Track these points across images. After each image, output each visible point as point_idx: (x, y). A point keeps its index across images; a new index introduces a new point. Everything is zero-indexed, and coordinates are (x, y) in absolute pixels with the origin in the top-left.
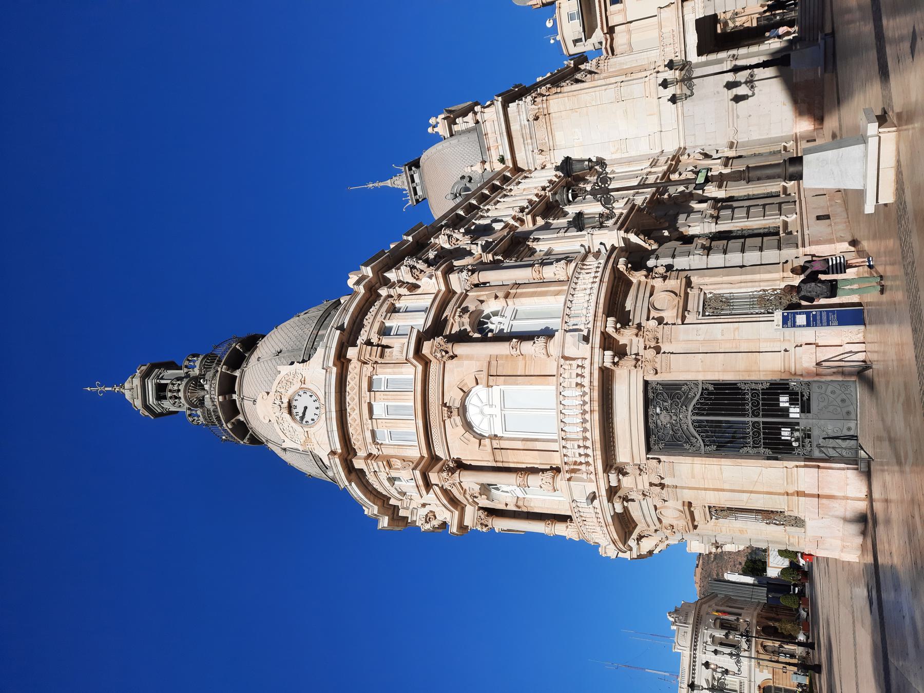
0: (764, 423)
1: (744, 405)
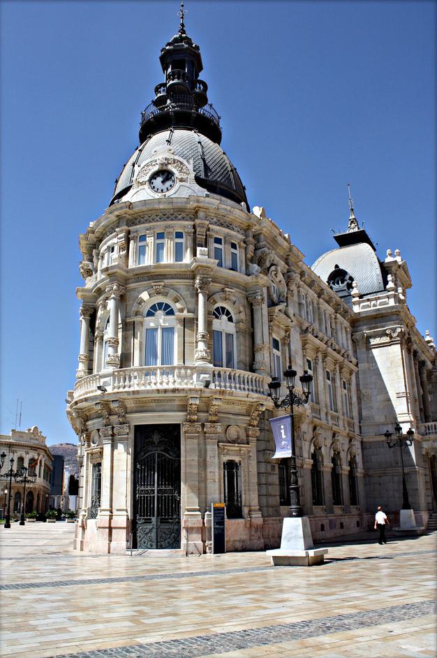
0: (154, 497)
1: (150, 485)
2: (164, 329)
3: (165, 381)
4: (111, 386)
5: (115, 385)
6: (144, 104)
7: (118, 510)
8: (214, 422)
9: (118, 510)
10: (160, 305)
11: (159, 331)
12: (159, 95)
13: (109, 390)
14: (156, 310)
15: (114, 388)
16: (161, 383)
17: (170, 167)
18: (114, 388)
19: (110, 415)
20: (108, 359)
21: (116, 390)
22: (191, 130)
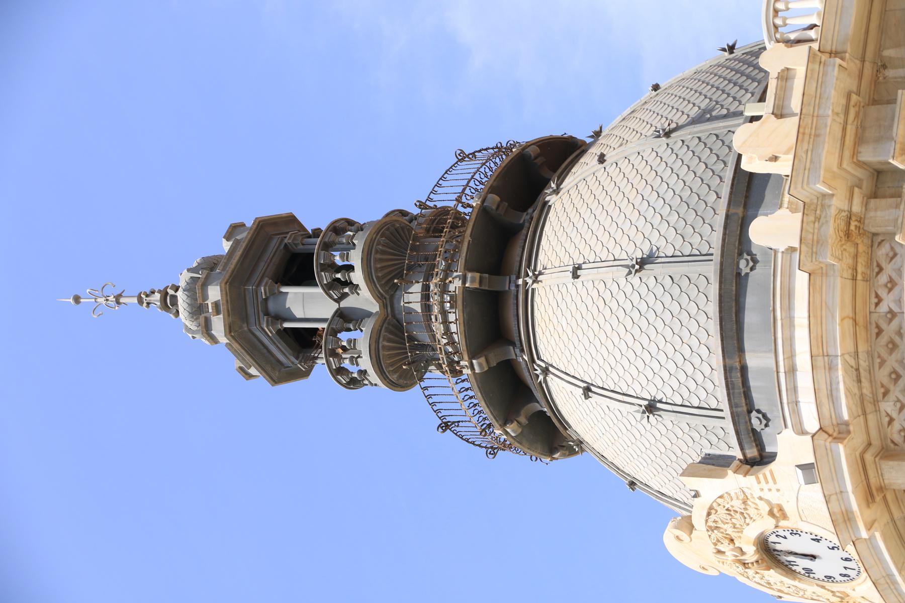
12: (357, 276)
17: (751, 553)
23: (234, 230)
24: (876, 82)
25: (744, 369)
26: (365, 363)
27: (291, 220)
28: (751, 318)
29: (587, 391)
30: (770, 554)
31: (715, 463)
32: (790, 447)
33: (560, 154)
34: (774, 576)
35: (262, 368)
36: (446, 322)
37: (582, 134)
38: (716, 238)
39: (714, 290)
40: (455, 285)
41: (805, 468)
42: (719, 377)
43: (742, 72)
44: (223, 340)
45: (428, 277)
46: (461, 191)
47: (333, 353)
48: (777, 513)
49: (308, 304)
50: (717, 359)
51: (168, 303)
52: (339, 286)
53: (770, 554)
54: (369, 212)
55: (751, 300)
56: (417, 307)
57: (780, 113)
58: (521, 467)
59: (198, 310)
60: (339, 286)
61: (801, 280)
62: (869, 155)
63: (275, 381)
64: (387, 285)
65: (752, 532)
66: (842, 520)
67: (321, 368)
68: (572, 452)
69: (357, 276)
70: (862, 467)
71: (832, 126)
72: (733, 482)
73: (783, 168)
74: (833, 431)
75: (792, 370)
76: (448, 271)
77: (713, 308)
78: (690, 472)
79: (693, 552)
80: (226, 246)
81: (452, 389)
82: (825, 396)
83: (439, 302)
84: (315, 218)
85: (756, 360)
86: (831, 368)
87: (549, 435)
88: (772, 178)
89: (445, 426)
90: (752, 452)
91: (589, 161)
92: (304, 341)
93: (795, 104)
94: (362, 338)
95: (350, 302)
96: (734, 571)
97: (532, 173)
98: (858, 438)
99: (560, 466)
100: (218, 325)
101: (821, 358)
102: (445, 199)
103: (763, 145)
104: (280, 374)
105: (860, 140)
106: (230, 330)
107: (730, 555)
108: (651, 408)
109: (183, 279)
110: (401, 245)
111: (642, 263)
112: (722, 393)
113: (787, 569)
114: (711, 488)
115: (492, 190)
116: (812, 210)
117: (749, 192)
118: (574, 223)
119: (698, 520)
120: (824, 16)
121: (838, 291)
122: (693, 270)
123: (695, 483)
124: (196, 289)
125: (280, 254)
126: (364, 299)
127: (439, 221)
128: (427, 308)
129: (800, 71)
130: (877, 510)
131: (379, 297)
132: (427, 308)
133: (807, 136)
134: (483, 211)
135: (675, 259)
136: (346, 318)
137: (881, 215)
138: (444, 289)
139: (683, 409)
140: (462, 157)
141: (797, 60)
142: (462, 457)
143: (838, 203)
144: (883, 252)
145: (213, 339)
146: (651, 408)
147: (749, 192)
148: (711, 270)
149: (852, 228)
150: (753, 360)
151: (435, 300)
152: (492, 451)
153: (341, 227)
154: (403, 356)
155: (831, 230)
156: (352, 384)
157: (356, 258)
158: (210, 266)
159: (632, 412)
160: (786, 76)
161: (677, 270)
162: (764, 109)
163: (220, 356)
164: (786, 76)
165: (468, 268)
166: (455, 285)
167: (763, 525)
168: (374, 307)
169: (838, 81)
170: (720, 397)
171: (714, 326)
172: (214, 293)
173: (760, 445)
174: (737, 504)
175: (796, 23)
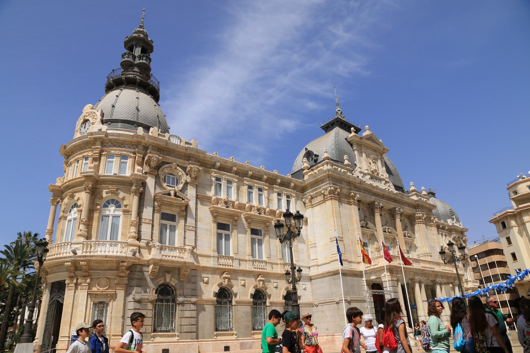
2: (114, 217)
3: (103, 250)
4: (81, 251)
5: (84, 250)
6: (113, 65)
7: (114, 336)
8: (123, 277)
9: (114, 336)
10: (113, 200)
11: (111, 218)
12: (141, 61)
13: (79, 253)
14: (109, 204)
15: (83, 253)
16: (121, 252)
17: (87, 118)
18: (83, 253)
19: (76, 270)
20: (80, 233)
21: (84, 254)
22: (148, 95)
23: (152, 41)
24: (161, 149)
25: (118, 122)
26: (126, 59)
27: (152, 51)
28: (127, 125)
29: (117, 96)
30: (86, 121)
31: (103, 115)
32: (104, 128)
33: (156, 98)
34: (82, 121)
35: (127, 41)
36: (132, 74)
37: (159, 102)
38: (140, 122)
39: (132, 120)
40: (138, 77)
41: (101, 130)
42: (117, 118)
43: (165, 130)
44: (133, 35)
45: (140, 73)
46: (153, 81)
47: (129, 53)
48: (93, 124)
49: (137, 51)
50: (120, 118)
51: (141, 27)
52: (140, 57)
53: (86, 121)
54: (152, 65)
55: (129, 125)
56: (135, 70)
57: (159, 135)
58: (104, 82)
59: (139, 32)
60: (140, 57)
61: (132, 134)
62: (150, 147)
63: (125, 42)
64: (139, 66)
65: (90, 119)
66: (91, 134)
67: (126, 51)
68: (106, 91)
69: (141, 61)
70: (100, 138)
71: (156, 142)
72: (99, 118)
73: (150, 134)
74: (107, 135)
75: (117, 130)
76: (140, 77)
77: (129, 119)
78: (102, 111)
79: (87, 108)
80: (150, 39)
81: (119, 73)
82: (113, 135)
83: (134, 74)
84: (152, 55)
85: (119, 124)
86: (117, 136)
87: (110, 88)
88: (145, 281)
89: (113, 71)
90: (104, 121)
91: (155, 103)
92: (131, 49)
93: (160, 137)
94: (130, 59)
95: (137, 59)
96: (83, 114)
97: (154, 94)
98: (105, 138)
99: (104, 89)
100: (136, 35)
101: (119, 135)
102: (152, 79)
103: (154, 131)
104: (126, 43)
105: (153, 146)
106: (135, 37)
107: (86, 115)
108: (113, 106)
109: (145, 31)
110: (145, 69)
111: (138, 109)
112: (114, 118)
113: (83, 123)
114: (99, 114)
115: (153, 87)
116: (143, 137)
117: (147, 128)
118: (145, 99)
119: (93, 110)
120: (172, 143)
121: (130, 139)
122: (136, 117)
123: (100, 111)
124: (142, 32)
125: (148, 49)
126: (137, 61)
127: (148, 77)
128: (134, 72)
129: (165, 139)
130: (92, 139)
131: (137, 64)
132: (134, 72)
133: (154, 138)
134: (150, 85)
135: (138, 114)
136: (134, 57)
137: (141, 147)
138: (137, 75)
139: (112, 111)
140: (159, 83)
141: (166, 138)
142: (107, 72)
143: (144, 141)
144: (135, 147)
145: (134, 33)
146: (113, 106)
147: (147, 128)
148: (135, 120)
149: (104, 345)
150: (119, 124)
151: (135, 73)
152: (108, 77)
153: (150, 60)
154: (127, 66)
155: (140, 140)
156: (123, 56)
157: (144, 61)
158: (146, 36)
159: (113, 102)
160: (164, 136)
161: (136, 114)
162: (159, 132)
163: (131, 33)
164: (164, 136)
165: (140, 80)
166: (138, 77)
167: (91, 121)
168: (136, 63)
169: (162, 144)
170: (114, 118)
171: (126, 119)
172: (142, 36)
173: (105, 123)
174: (95, 117)
175: (172, 139)
